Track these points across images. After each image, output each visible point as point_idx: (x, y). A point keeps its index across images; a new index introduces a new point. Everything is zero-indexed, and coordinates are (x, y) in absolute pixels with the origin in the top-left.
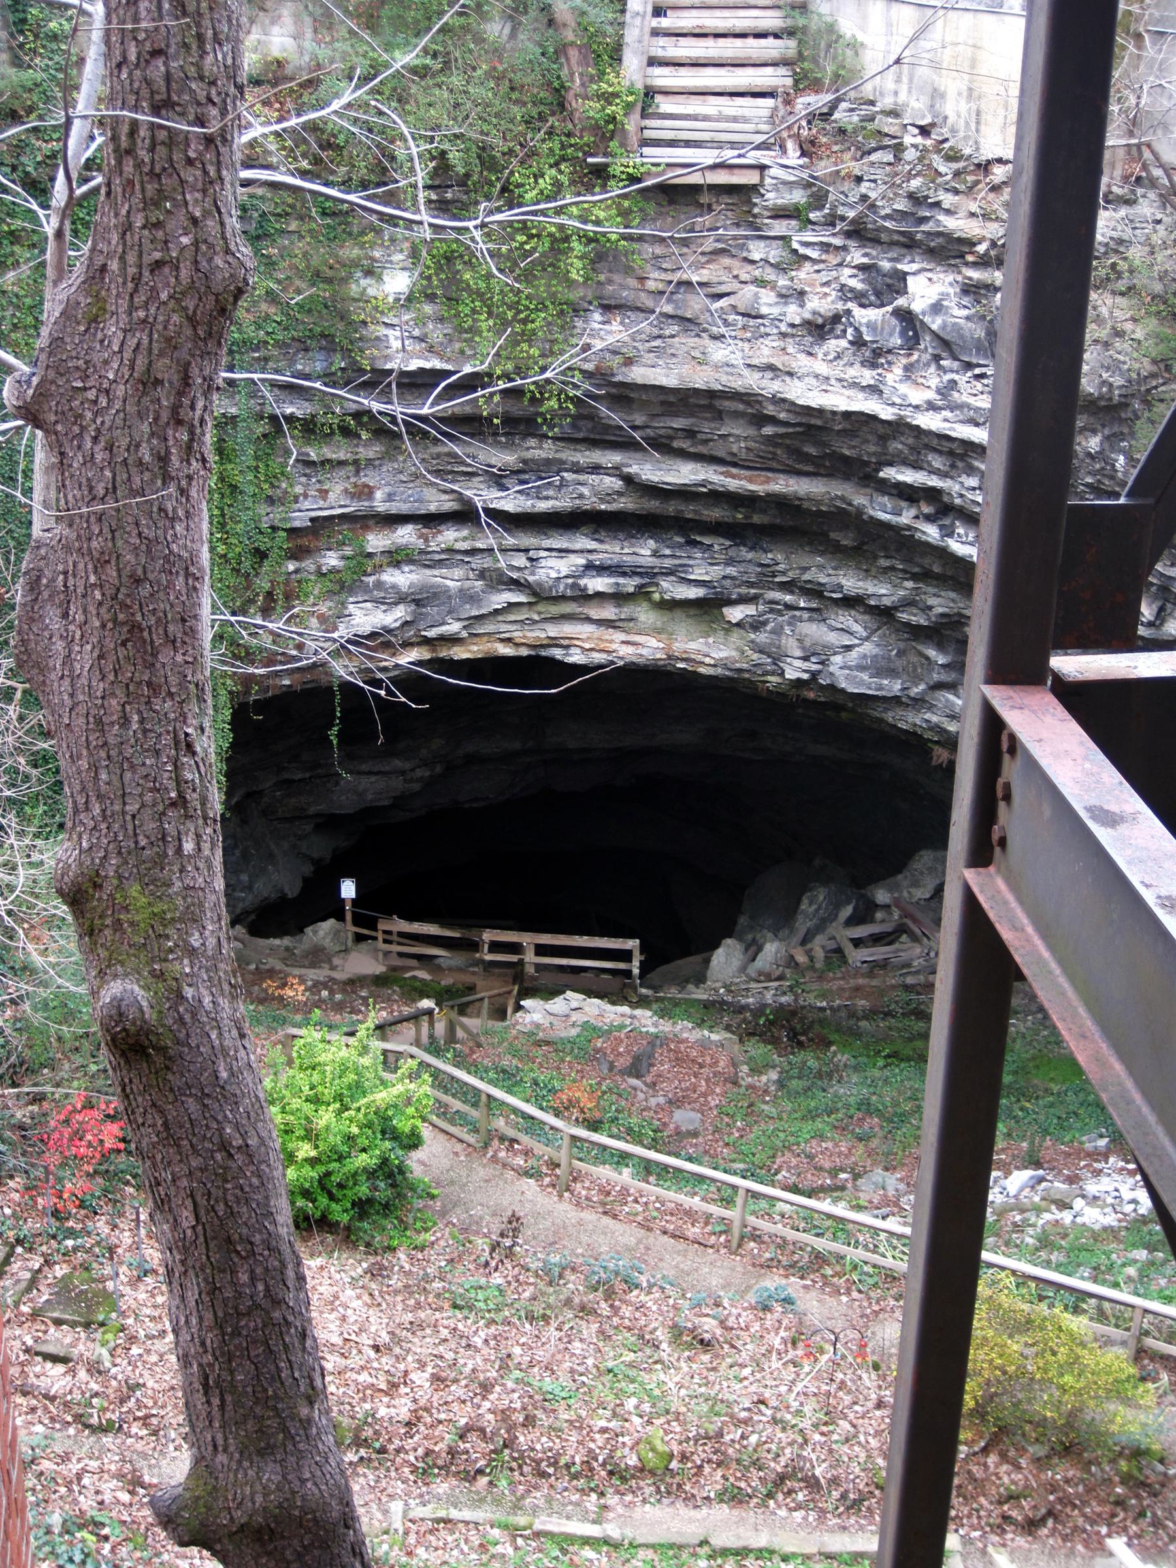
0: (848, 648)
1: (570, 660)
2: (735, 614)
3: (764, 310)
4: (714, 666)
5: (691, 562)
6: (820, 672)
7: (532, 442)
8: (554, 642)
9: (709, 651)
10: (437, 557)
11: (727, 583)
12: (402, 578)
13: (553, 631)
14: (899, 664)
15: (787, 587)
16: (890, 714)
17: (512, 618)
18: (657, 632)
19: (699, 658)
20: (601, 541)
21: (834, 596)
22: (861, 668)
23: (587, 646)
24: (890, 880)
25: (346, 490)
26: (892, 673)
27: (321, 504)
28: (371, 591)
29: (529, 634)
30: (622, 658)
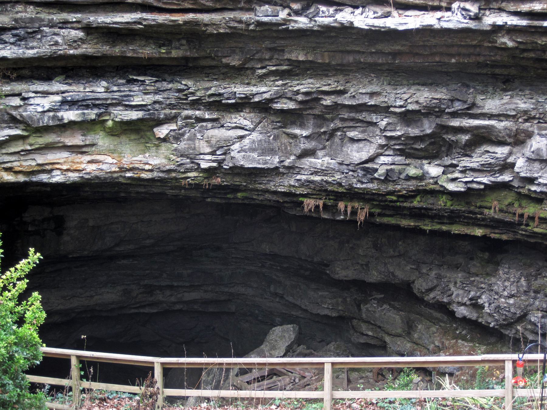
0: (242, 137)
1: (54, 180)
2: (162, 131)
4: (151, 171)
5: (132, 93)
6: (224, 160)
8: (42, 169)
9: (149, 161)
11: (157, 106)
13: (40, 159)
14: (276, 145)
15: (196, 104)
16: (272, 183)
17: (12, 150)
18: (111, 152)
19: (141, 166)
20: (70, 85)
21: (230, 101)
22: (253, 150)
23: (65, 167)
26: (272, 152)
29: (24, 164)
30: (89, 173)
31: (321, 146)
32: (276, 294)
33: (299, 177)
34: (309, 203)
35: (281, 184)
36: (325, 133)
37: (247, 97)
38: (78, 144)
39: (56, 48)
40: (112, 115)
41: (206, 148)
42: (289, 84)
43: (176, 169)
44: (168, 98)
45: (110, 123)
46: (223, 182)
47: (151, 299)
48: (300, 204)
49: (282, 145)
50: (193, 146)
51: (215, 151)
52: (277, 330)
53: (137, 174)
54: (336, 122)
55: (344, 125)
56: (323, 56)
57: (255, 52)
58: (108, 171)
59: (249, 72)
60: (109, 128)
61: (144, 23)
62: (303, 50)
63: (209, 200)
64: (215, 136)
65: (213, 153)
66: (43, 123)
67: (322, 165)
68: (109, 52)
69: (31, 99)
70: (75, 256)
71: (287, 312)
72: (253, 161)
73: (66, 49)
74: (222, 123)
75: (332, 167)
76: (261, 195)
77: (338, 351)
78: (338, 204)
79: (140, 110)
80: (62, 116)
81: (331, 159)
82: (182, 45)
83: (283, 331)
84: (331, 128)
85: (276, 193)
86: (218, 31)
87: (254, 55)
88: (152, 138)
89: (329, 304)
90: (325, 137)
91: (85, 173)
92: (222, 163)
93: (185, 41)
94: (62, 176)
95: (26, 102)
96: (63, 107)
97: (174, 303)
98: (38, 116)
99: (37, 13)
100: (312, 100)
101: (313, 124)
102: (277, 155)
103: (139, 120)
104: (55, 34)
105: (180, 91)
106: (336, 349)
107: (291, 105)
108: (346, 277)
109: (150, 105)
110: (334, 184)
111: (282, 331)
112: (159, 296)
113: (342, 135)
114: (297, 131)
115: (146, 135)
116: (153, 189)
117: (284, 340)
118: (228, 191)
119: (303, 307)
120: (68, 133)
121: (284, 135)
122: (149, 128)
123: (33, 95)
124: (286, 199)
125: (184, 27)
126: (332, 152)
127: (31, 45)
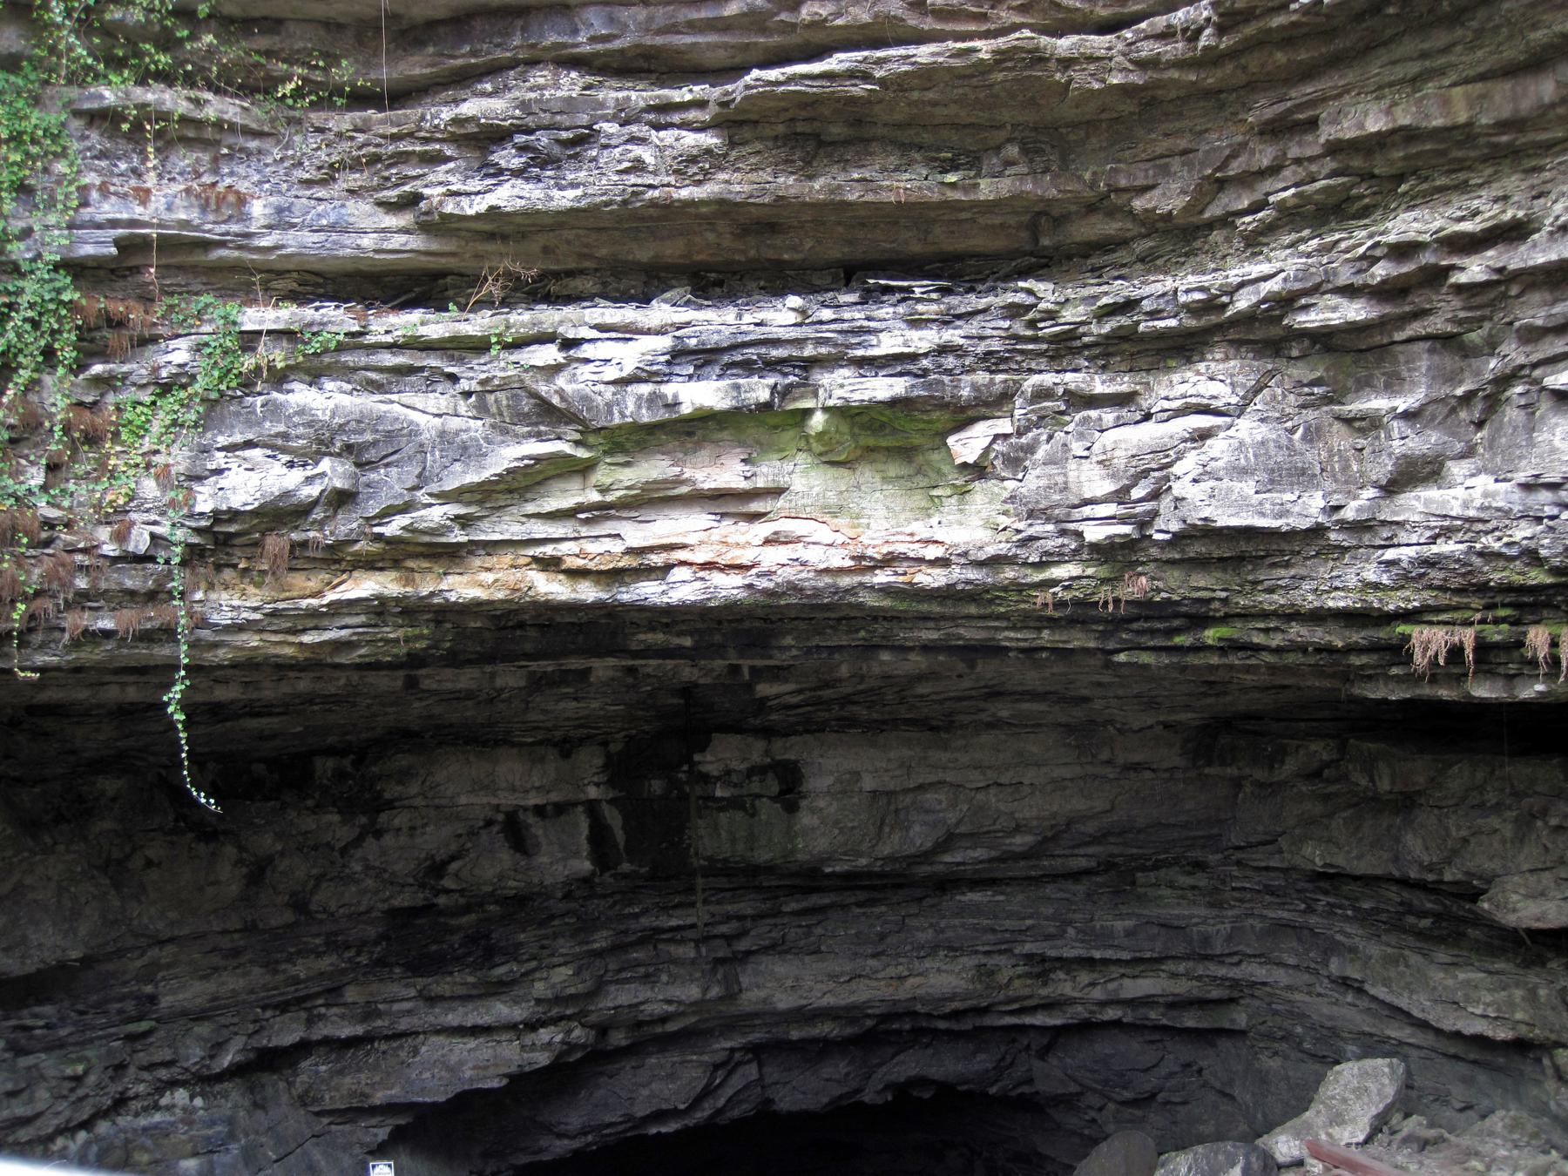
0: (1203, 436)
2: (969, 445)
4: (942, 562)
5: (872, 324)
7: (540, 77)
9: (934, 532)
10: (388, 359)
11: (950, 361)
12: (324, 401)
13: (636, 534)
14: (1313, 457)
15: (1064, 348)
16: (1306, 586)
17: (552, 504)
22: (1242, 472)
23: (700, 557)
24: (1296, 1122)
25: (188, 191)
26: (1302, 477)
27: (138, 212)
28: (259, 424)
29: (592, 548)
30: (768, 574)
31: (1459, 447)
32: (1345, 983)
33: (1390, 554)
34: (1430, 640)
35: (1337, 583)
36: (1468, 398)
37: (1212, 305)
38: (733, 485)
39: (639, 181)
40: (821, 391)
41: (1100, 483)
42: (1343, 245)
43: (1016, 556)
44: (982, 338)
45: (818, 421)
46: (1158, 590)
47: (1044, 992)
48: (1399, 651)
49: (1331, 456)
50: (1060, 479)
51: (1126, 490)
52: (1348, 1072)
53: (905, 574)
54: (1504, 349)
55: (1535, 358)
56: (1446, 102)
57: (1227, 152)
58: (822, 566)
59: (1217, 236)
60: (820, 435)
61: (878, 74)
62: (1377, 98)
63: (1122, 657)
64: (1125, 441)
65: (1120, 496)
66: (623, 415)
67: (1466, 505)
68: (792, 191)
69: (585, 346)
70: (838, 869)
71: (1373, 1030)
72: (1240, 506)
73: (668, 185)
74: (1145, 405)
75: (1501, 504)
76: (1276, 629)
77: (1516, 1136)
78: (1525, 634)
79: (901, 374)
80: (675, 396)
81: (1497, 481)
82: (1009, 163)
83: (1364, 1074)
84: (1489, 376)
85: (1319, 616)
86: (1103, 81)
87: (1224, 166)
88: (946, 469)
89: (1488, 1005)
90: (1471, 412)
91: (758, 576)
92: (1149, 524)
93: (1016, 150)
94: (698, 585)
95: (571, 352)
96: (677, 370)
97: (1103, 1004)
98: (608, 396)
99: (588, 87)
100: (1415, 282)
101: (1429, 369)
102: (1317, 487)
103: (894, 402)
104: (633, 140)
105: (1014, 311)
106: (1515, 1126)
107: (1355, 311)
108: (1538, 920)
109: (926, 355)
110: (1512, 559)
111: (1361, 1076)
112: (1063, 986)
113: (1528, 392)
114: (1378, 403)
115: (929, 463)
116: (962, 631)
117: (1366, 1100)
118: (1176, 623)
119: (1416, 1013)
120: (704, 454)
121: (1337, 426)
122: (937, 440)
123: (595, 334)
124: (1358, 637)
125: (1000, 76)
126: (1499, 460)
127: (570, 176)
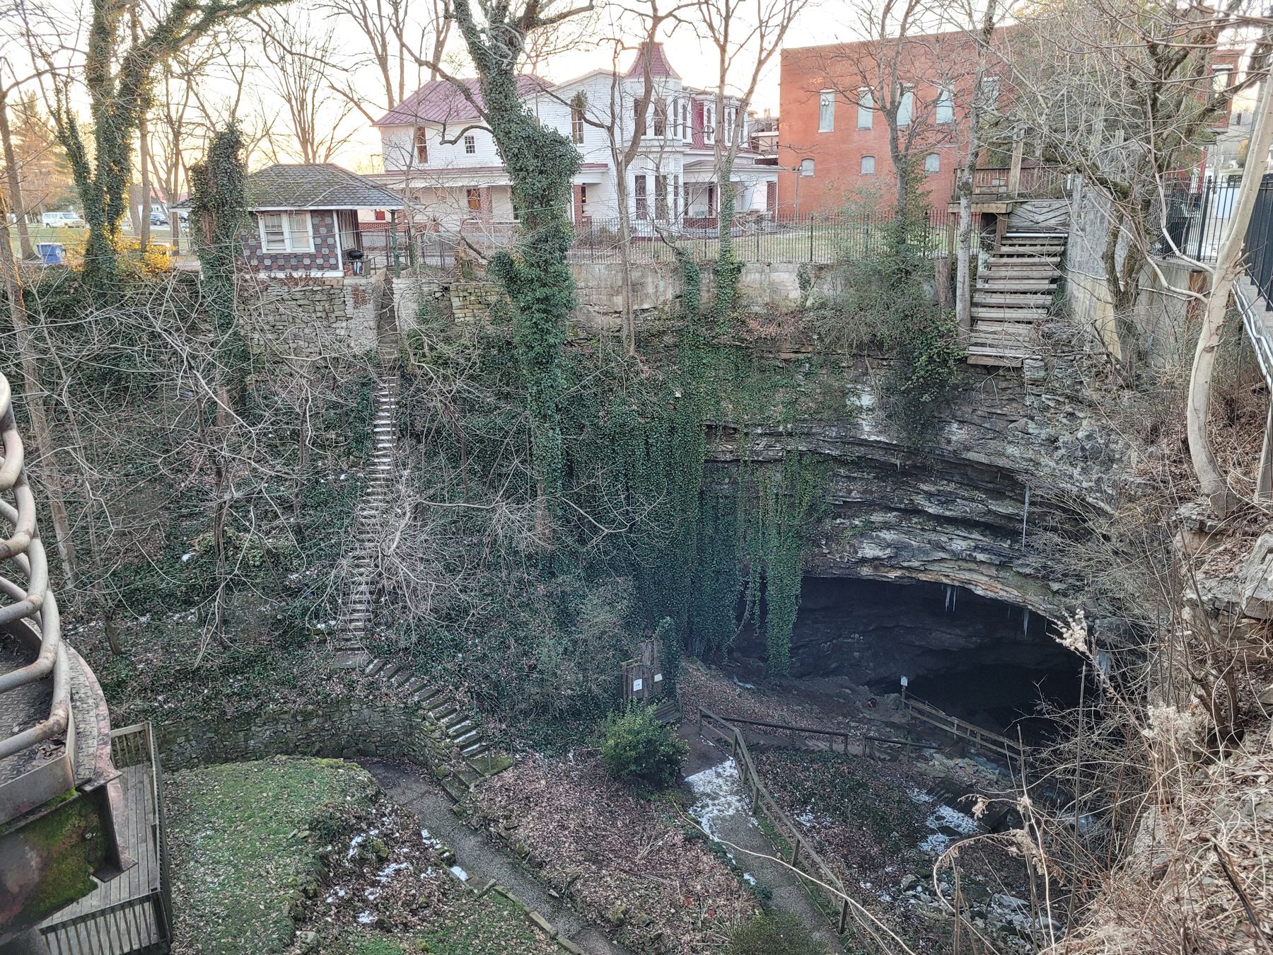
3: (1031, 431)
12: (888, 536)
18: (1017, 588)
